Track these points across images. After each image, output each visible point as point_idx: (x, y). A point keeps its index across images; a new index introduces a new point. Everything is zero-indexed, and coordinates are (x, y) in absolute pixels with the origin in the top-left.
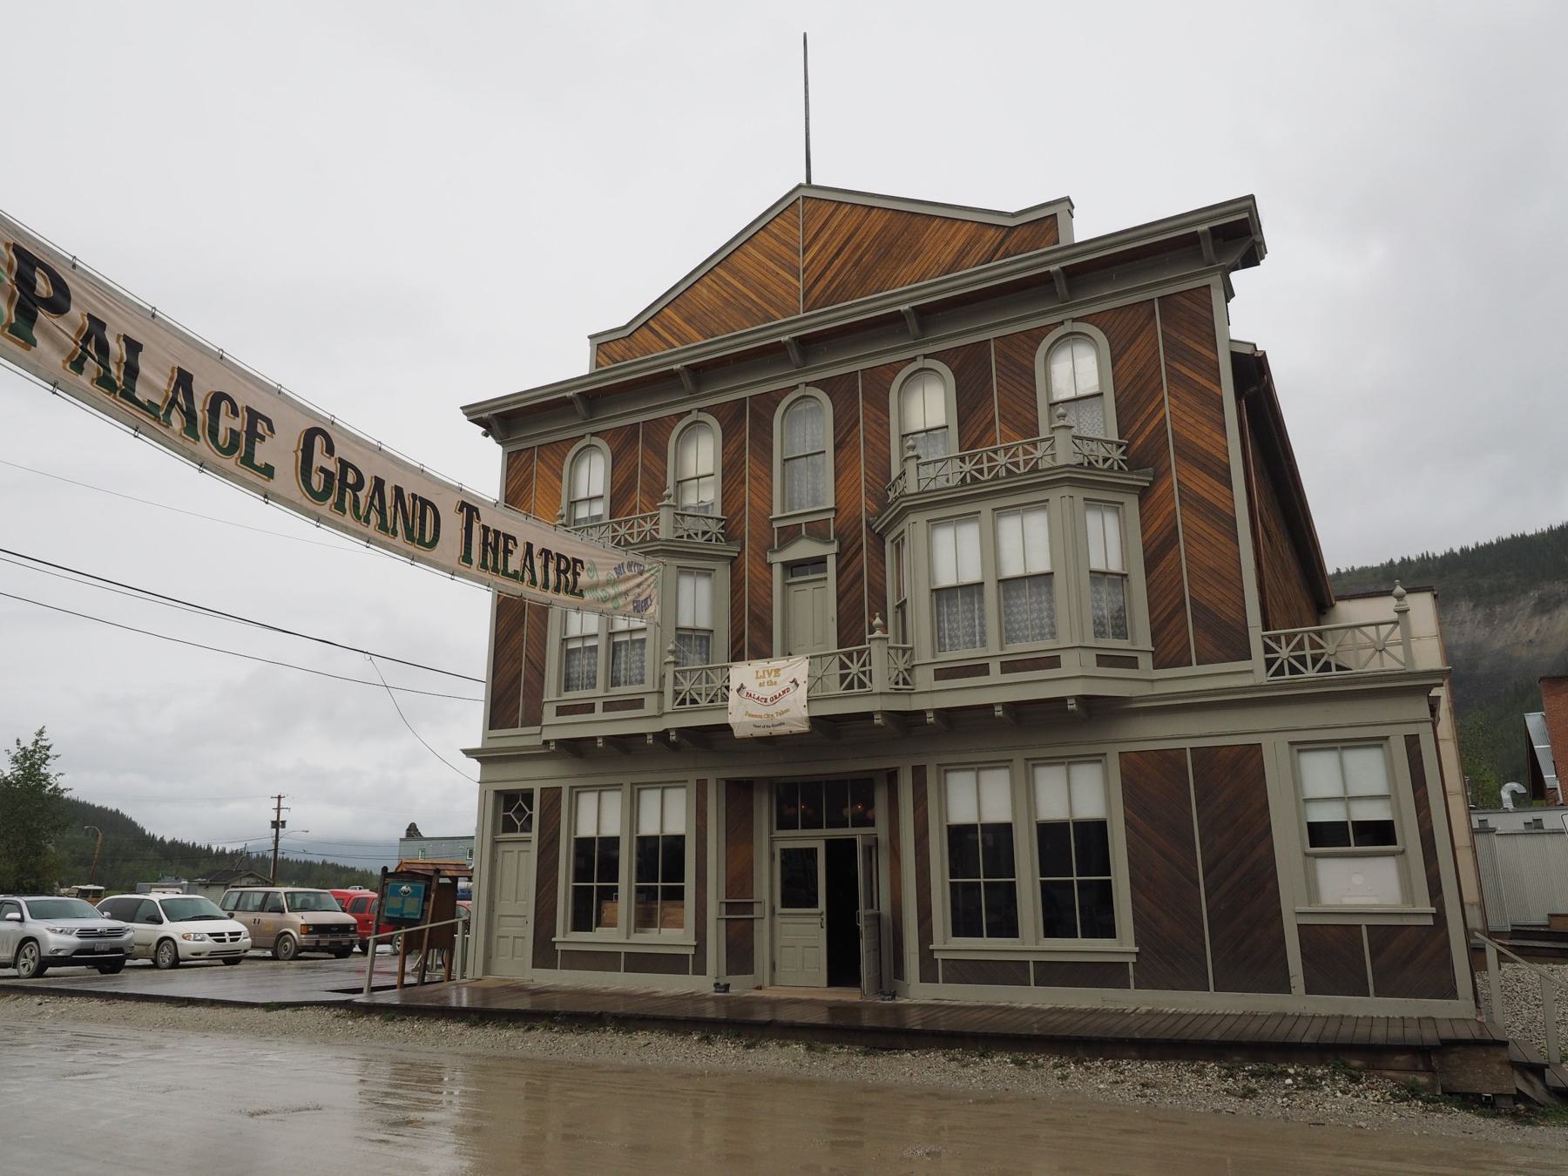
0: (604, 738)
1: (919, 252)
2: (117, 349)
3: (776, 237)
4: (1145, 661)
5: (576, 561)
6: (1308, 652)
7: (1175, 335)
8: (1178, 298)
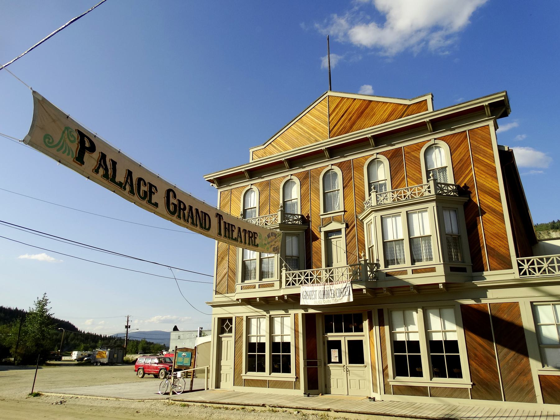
0: (260, 298)
1: (374, 114)
2: (109, 163)
3: (319, 111)
5: (255, 233)
7: (475, 144)
8: (476, 130)
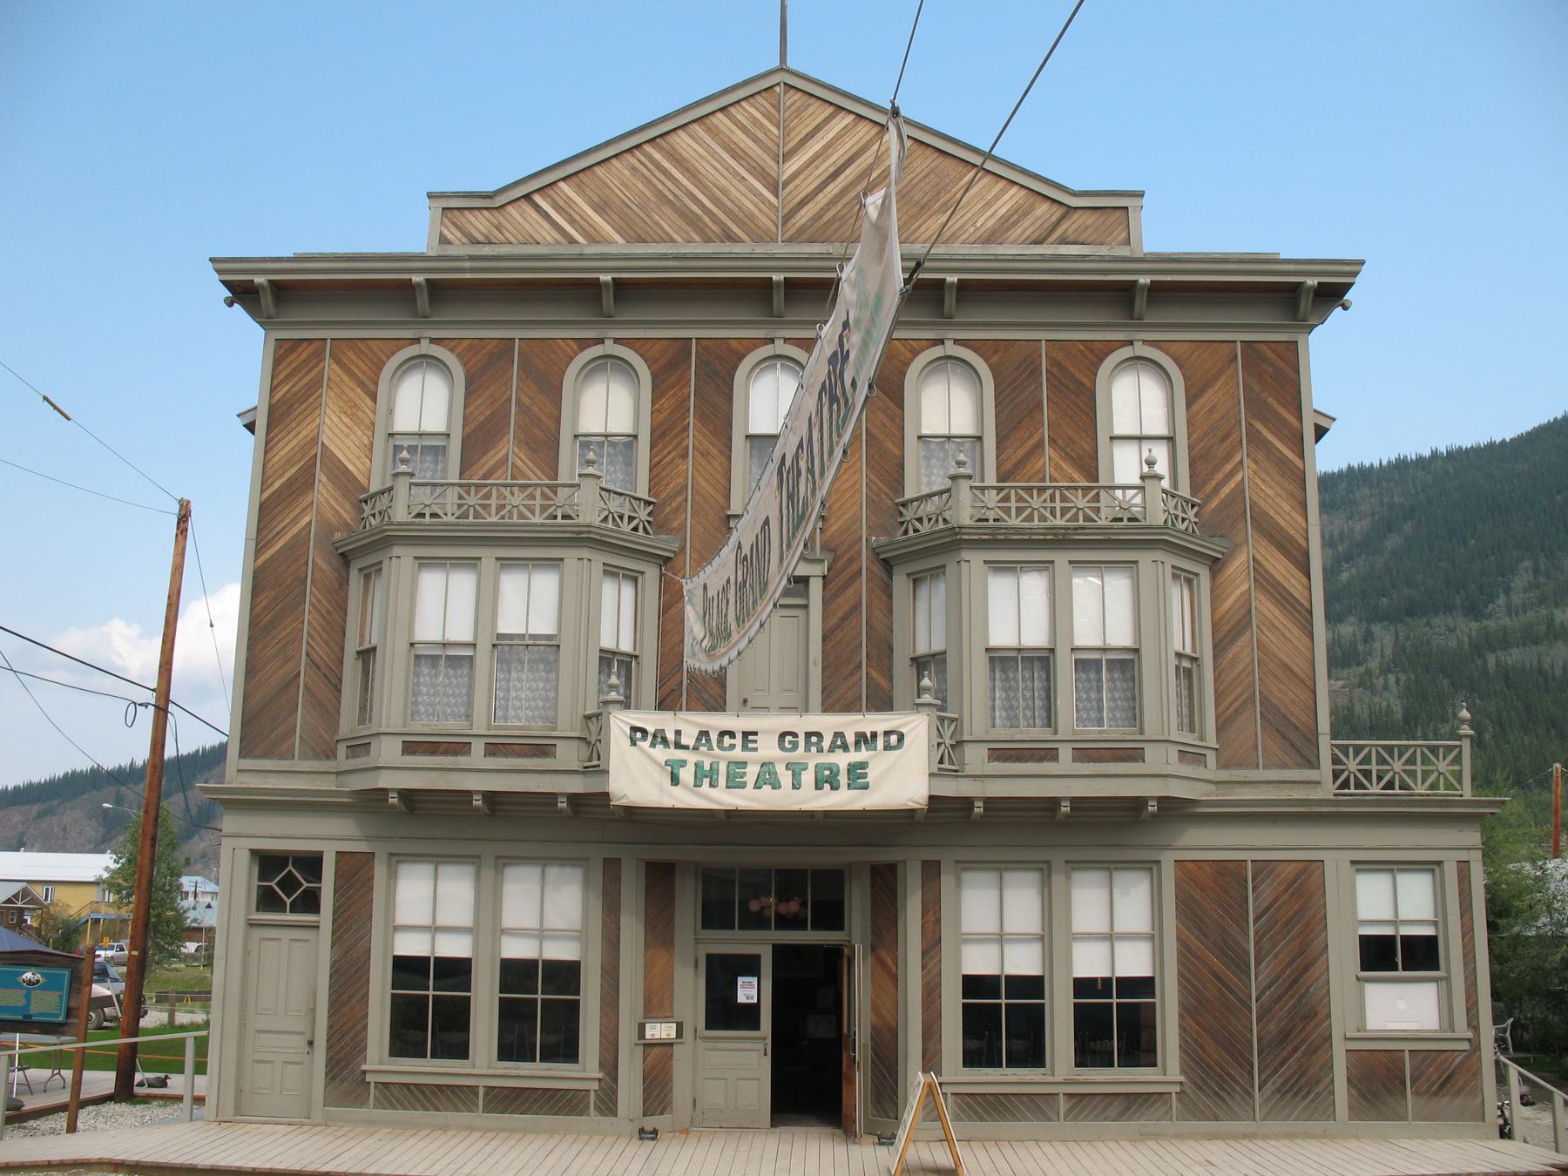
4: (1211, 758)
6: (1374, 767)
8: (1263, 347)
